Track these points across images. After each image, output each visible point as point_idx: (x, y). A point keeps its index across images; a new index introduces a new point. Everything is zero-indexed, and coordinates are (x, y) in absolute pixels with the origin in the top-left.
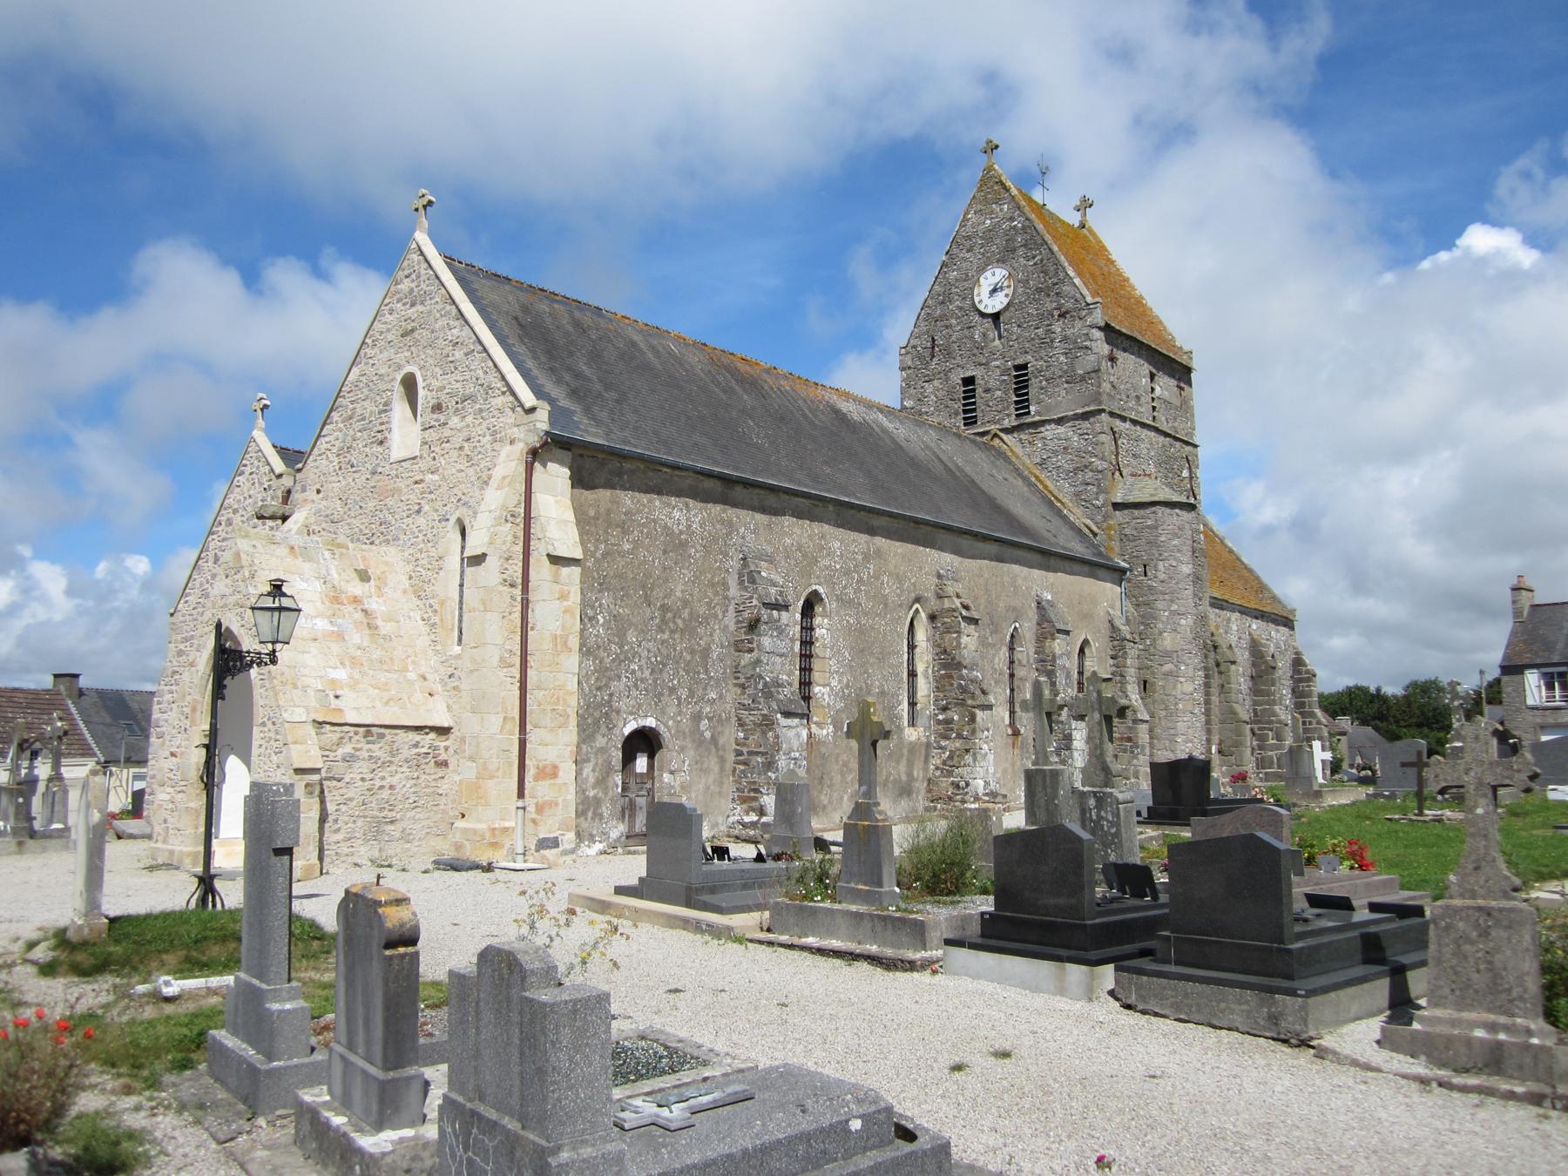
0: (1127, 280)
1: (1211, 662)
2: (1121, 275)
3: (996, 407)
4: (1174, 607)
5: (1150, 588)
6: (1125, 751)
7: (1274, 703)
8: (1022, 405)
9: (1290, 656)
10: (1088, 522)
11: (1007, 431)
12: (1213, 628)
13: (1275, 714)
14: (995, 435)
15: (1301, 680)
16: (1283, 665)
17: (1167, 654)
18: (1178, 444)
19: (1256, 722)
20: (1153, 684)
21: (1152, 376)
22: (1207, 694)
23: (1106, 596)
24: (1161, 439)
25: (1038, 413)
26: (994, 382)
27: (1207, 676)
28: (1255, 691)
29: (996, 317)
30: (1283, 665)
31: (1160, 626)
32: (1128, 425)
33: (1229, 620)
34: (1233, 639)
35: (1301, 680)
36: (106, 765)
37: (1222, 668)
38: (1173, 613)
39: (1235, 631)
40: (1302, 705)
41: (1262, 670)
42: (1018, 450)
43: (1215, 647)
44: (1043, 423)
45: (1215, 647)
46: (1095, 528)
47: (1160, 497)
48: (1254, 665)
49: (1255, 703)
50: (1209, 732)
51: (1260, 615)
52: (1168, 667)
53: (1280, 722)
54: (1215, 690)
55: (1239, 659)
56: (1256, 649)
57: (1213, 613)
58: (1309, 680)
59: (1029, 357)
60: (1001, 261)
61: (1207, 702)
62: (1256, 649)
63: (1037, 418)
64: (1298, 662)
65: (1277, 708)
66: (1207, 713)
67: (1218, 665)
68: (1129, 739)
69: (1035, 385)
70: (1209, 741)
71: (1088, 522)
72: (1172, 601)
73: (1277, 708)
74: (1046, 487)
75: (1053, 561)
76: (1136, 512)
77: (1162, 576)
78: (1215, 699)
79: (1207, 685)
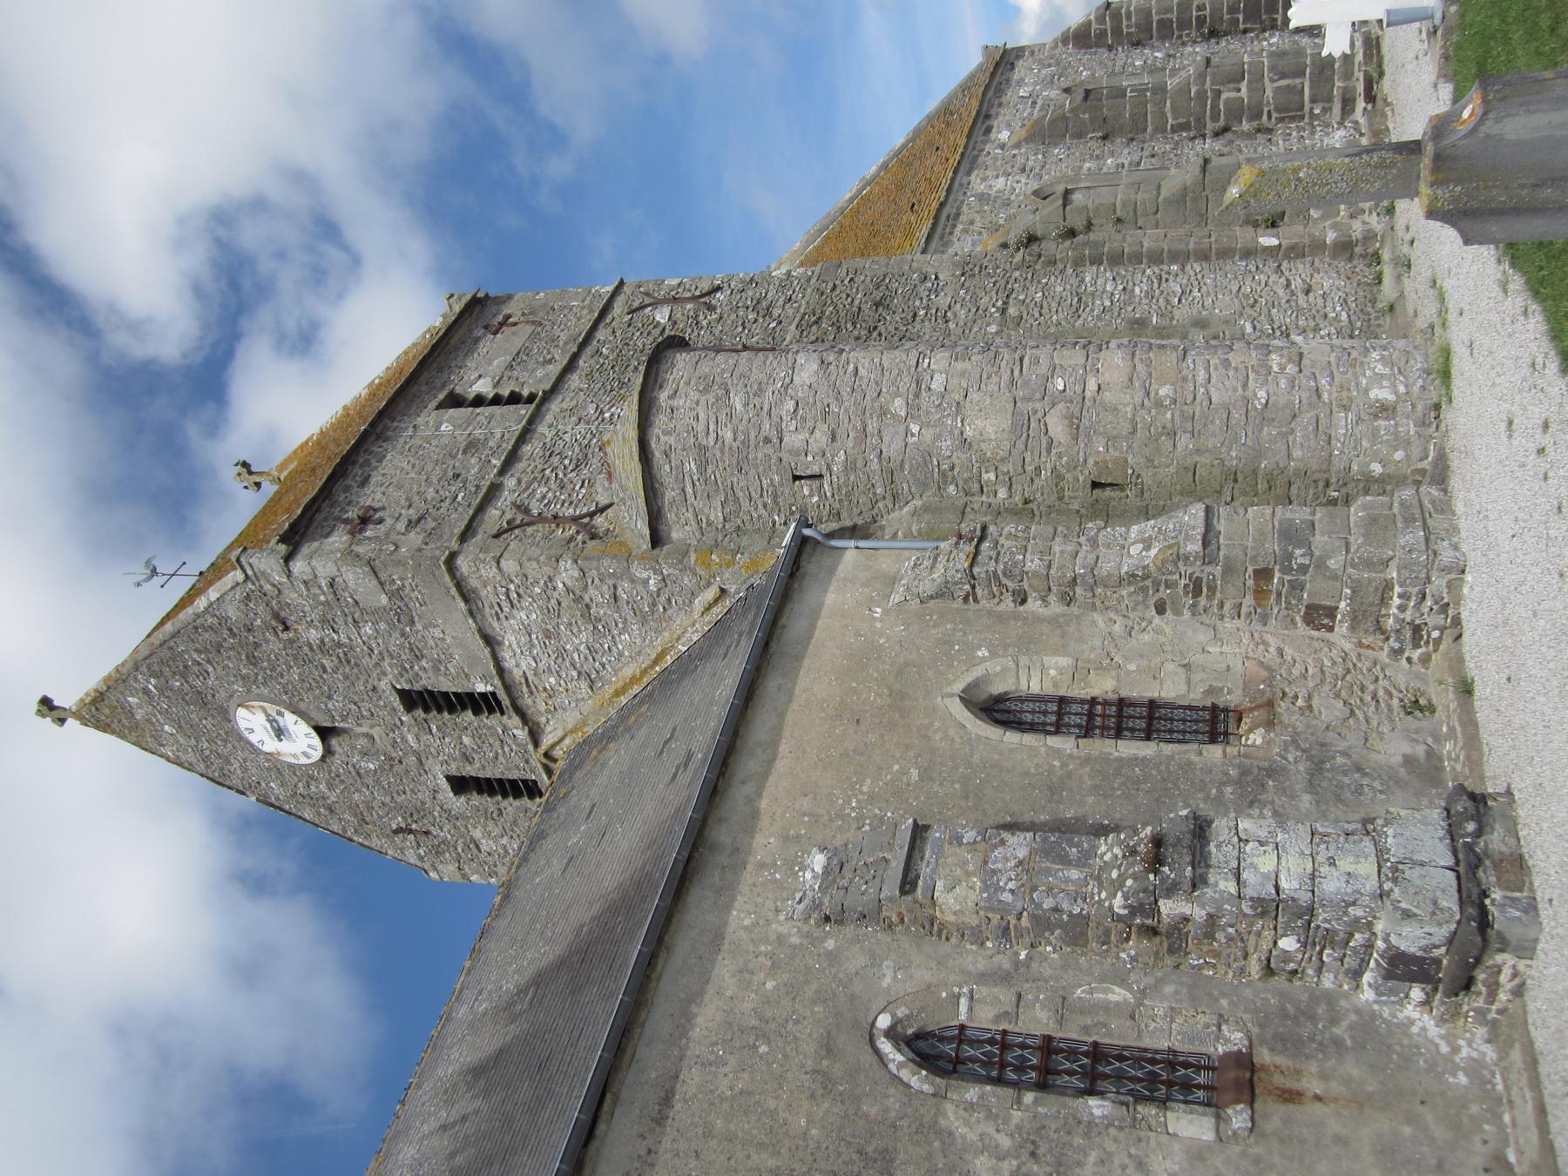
0: (346, 408)
1: (1065, 250)
2: (339, 421)
3: (497, 746)
4: (898, 406)
5: (850, 466)
6: (1297, 587)
7: (1160, 89)
8: (483, 704)
9: (1070, 53)
10: (699, 603)
11: (535, 736)
12: (992, 244)
13: (1184, 89)
14: (546, 755)
15: (1117, 31)
16: (1088, 69)
17: (1022, 426)
18: (601, 334)
19: (1201, 123)
20: (1102, 466)
21: (455, 401)
22: (1137, 258)
23: (854, 603)
24: (575, 380)
25: (485, 678)
26: (452, 744)
27: (1096, 261)
28: (1135, 131)
29: (324, 733)
30: (1088, 69)
31: (946, 444)
32: (510, 482)
33: (983, 198)
34: (1025, 186)
35: (1117, 31)
36: (1208, 866)
37: (1078, 223)
38: (913, 410)
39: (1005, 184)
40: (1165, 25)
41: (1094, 116)
42: (571, 718)
43: (1032, 239)
44: (501, 671)
45: (1032, 239)
46: (710, 594)
47: (633, 434)
48: (1079, 135)
49: (1161, 129)
50: (1225, 254)
51: (983, 119)
52: (1057, 427)
53: (1201, 77)
54: (1129, 240)
55: (1066, 168)
56: (1047, 133)
57: (963, 244)
58: (1116, 17)
59: (383, 685)
60: (226, 715)
61: (1156, 258)
62: (1047, 133)
63: (497, 681)
64: (1081, 38)
65: (1171, 83)
66: (1181, 257)
67: (1071, 233)
68: (1263, 574)
69: (430, 681)
70: (1248, 254)
71: (699, 603)
72: (884, 412)
73: (1171, 83)
74: (634, 680)
75: (721, 834)
76: (670, 495)
77: (820, 437)
78: (1149, 240)
79: (1117, 259)
